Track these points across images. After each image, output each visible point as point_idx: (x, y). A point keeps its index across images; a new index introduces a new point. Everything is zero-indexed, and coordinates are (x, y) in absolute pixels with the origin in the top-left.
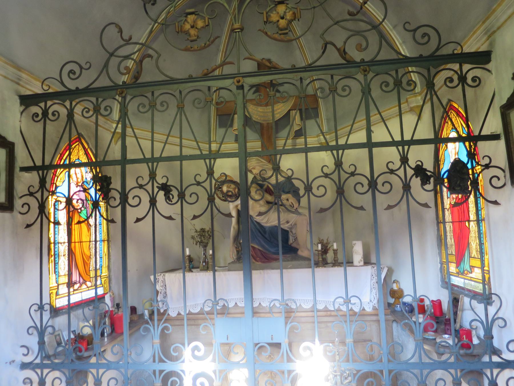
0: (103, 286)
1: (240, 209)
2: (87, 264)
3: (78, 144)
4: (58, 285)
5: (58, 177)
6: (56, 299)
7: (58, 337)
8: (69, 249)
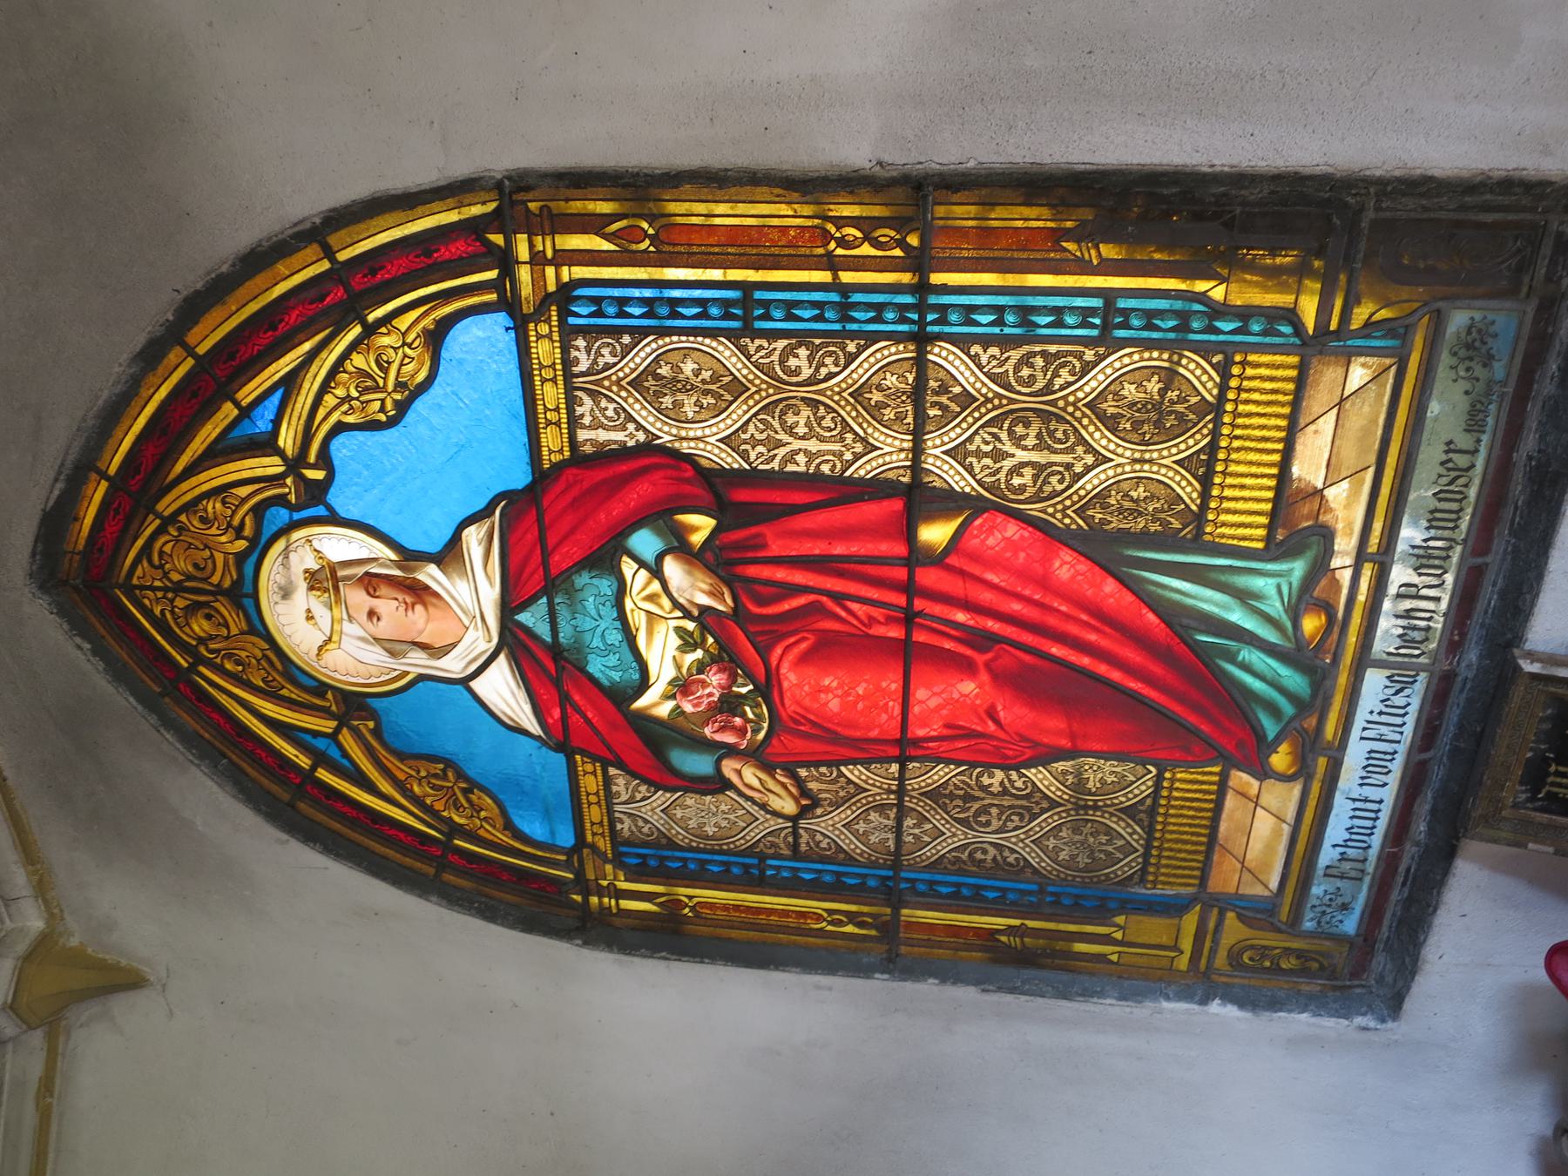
3: (130, 590)
5: (455, 830)
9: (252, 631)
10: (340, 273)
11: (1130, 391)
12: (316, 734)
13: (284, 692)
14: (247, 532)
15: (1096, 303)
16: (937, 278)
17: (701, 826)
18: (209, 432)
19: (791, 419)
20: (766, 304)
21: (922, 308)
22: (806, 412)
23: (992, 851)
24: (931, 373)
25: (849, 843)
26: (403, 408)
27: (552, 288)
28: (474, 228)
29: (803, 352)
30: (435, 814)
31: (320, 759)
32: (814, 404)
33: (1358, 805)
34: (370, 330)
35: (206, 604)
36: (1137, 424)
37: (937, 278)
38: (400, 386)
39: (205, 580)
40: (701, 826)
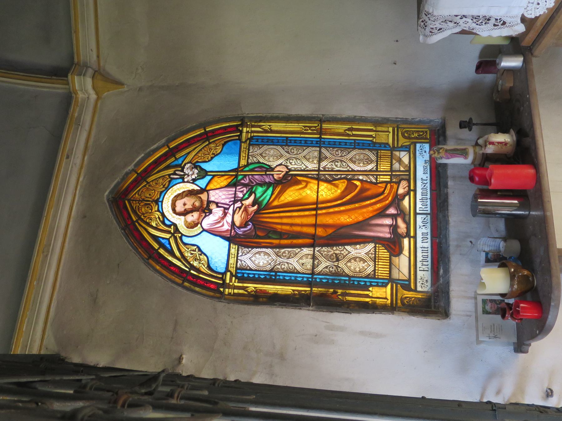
0: (415, 144)
1: (80, 416)
2: (363, 190)
3: (129, 201)
4: (391, 280)
5: (192, 267)
6: (415, 290)
7: (488, 308)
8: (327, 245)
9: (158, 211)
10: (206, 133)
11: (357, 157)
12: (163, 238)
13: (160, 228)
14: (166, 186)
15: (353, 141)
16: (323, 137)
17: (355, 269)
18: (168, 162)
19: (337, 164)
20: (291, 140)
21: (320, 141)
22: (295, 160)
23: (286, 264)
24: (322, 154)
25: (299, 268)
26: (212, 158)
27: (249, 136)
28: (237, 126)
29: (295, 149)
30: (189, 263)
31: (162, 245)
32: (341, 161)
33: (423, 249)
34: (210, 143)
35: (149, 204)
36: (367, 162)
37: (323, 137)
38: (213, 154)
39: (150, 198)
40: (355, 269)
